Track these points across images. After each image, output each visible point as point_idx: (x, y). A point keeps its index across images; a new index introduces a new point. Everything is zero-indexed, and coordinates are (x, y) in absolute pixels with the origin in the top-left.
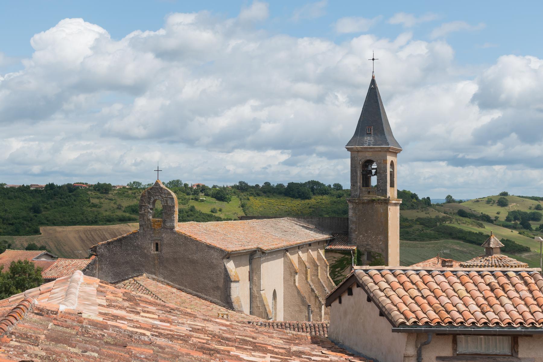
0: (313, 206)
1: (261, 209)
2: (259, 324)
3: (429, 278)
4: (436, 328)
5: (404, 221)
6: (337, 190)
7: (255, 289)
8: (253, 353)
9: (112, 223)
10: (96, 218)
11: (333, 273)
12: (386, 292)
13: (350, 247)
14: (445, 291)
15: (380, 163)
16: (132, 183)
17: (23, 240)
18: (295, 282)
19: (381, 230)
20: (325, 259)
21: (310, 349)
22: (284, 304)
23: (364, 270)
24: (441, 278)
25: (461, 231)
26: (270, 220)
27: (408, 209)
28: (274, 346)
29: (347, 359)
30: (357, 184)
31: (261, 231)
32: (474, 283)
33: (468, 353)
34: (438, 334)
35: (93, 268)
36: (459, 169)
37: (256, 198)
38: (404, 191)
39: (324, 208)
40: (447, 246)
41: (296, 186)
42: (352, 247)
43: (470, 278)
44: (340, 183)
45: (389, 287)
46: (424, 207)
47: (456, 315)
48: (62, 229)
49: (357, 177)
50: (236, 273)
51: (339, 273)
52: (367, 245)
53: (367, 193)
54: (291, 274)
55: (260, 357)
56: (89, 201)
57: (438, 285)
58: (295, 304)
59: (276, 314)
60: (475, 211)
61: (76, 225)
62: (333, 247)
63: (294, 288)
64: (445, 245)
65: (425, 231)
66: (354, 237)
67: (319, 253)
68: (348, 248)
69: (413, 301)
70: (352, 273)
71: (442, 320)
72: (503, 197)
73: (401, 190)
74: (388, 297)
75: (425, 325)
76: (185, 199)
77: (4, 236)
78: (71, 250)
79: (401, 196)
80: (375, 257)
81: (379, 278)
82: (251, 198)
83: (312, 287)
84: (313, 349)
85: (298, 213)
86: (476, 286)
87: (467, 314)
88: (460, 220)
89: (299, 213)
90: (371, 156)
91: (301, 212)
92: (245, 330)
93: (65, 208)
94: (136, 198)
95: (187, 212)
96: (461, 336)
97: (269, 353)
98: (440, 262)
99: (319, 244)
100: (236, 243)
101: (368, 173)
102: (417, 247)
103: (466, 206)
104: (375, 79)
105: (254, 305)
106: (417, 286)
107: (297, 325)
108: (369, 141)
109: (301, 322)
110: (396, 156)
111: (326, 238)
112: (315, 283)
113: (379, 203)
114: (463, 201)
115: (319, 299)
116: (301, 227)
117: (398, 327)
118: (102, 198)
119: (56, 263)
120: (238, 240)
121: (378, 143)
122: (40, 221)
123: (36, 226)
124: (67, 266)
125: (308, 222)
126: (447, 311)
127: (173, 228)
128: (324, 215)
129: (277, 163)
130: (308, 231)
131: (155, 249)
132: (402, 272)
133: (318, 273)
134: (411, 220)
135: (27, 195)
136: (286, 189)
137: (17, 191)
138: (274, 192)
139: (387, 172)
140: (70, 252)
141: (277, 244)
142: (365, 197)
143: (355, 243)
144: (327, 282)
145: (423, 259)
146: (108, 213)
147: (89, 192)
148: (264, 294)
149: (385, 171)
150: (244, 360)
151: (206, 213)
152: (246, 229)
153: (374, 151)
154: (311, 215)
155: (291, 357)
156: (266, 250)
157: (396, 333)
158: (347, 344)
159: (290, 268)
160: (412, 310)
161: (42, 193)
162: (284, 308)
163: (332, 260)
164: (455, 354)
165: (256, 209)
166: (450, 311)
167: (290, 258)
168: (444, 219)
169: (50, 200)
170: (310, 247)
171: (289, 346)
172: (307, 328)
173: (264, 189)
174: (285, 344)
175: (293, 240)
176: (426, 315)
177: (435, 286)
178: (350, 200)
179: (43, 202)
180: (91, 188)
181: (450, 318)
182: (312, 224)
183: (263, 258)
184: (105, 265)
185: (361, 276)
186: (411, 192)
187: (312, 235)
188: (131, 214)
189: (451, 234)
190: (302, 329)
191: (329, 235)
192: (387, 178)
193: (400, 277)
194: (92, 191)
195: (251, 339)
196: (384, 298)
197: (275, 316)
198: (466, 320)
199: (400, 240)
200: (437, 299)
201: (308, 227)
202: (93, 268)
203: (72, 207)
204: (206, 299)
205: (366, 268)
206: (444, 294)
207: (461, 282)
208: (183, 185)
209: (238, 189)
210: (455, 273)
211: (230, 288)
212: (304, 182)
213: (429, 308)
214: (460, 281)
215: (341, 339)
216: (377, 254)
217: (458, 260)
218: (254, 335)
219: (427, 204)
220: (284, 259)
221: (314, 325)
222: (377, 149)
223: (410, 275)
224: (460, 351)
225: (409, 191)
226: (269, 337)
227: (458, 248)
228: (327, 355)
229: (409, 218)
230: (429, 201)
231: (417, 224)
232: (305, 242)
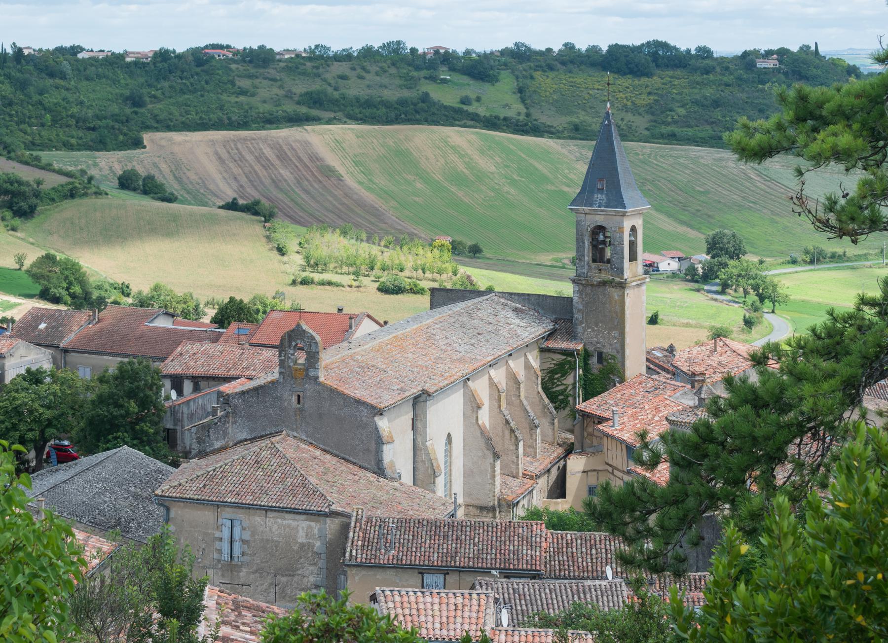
0: (656, 90)
1: (555, 97)
7: (419, 440)
9: (275, 125)
10: (245, 117)
16: (313, 47)
17: (113, 160)
37: (546, 74)
41: (624, 52)
48: (183, 138)
51: (558, 381)
56: (233, 83)
61: (209, 130)
63: (476, 426)
76: (412, 77)
77: (78, 153)
78: (200, 178)
79: (826, 71)
82: (537, 74)
83: (507, 418)
85: (626, 105)
89: (629, 103)
91: (632, 102)
93: (188, 96)
94: (319, 76)
95: (415, 105)
105: (419, 459)
118: (257, 77)
119: (179, 349)
122: (143, 123)
123: (136, 133)
124: (194, 354)
127: (317, 378)
131: (297, 402)
135: (119, 72)
137: (101, 65)
138: (582, 63)
140: (199, 184)
143: (582, 339)
146: (267, 107)
147: (233, 66)
148: (432, 445)
151: (451, 104)
154: (651, 108)
161: (147, 69)
165: (546, 96)
169: (162, 81)
172: (445, 526)
173: (563, 56)
179: (150, 86)
180: (236, 58)
188: (310, 108)
194: (238, 64)
203: (202, 96)
204: (354, 464)
208: (409, 51)
212: (638, 43)
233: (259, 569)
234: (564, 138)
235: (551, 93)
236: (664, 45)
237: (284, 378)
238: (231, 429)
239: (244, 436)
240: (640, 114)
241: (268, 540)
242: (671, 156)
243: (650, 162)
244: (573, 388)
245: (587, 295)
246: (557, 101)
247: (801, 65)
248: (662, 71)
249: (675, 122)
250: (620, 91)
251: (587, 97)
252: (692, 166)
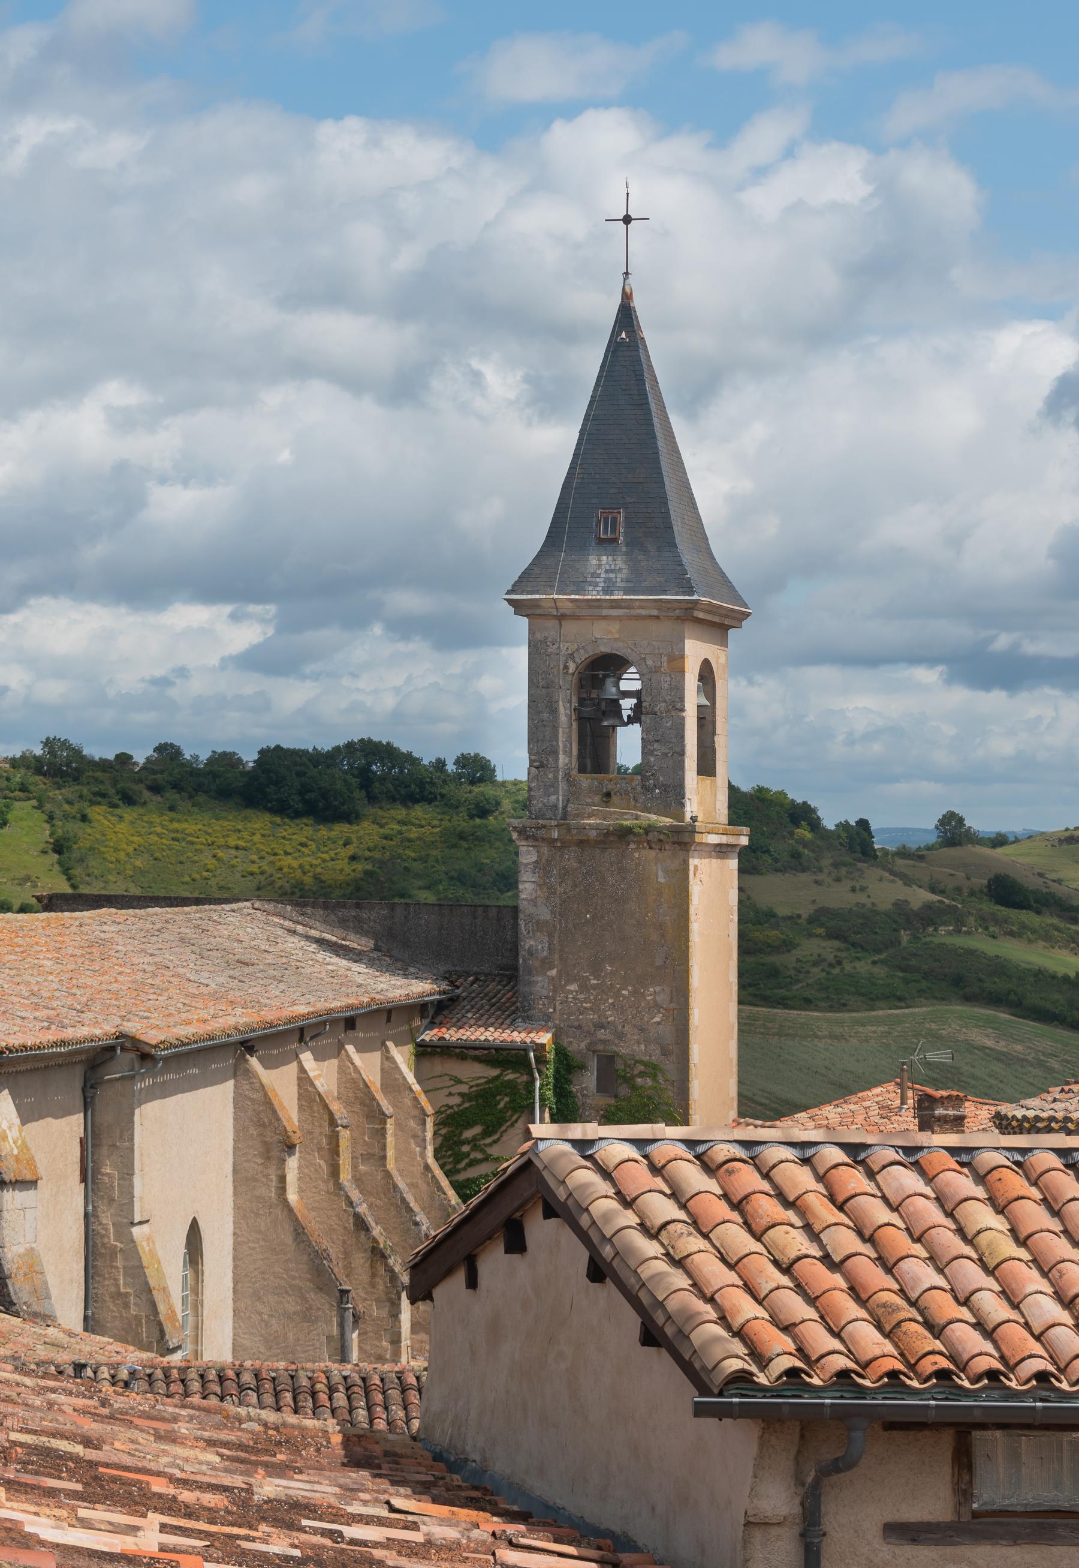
1: (138, 863)
2: (124, 1374)
3: (854, 1180)
4: (885, 1398)
5: (760, 924)
6: (472, 783)
7: (107, 1219)
8: (82, 1513)
11: (450, 1148)
12: (669, 1238)
13: (523, 1035)
14: (922, 1235)
15: (657, 670)
18: (282, 1189)
19: (659, 962)
20: (416, 1087)
21: (337, 1490)
22: (236, 1282)
23: (575, 1143)
24: (908, 1180)
25: (1000, 968)
26: (176, 914)
27: (777, 870)
28: (178, 1480)
29: (498, 1533)
30: (557, 760)
31: (135, 960)
32: (1045, 1200)
33: (1019, 1509)
34: (891, 1426)
36: (995, 699)
37: (118, 811)
38: (760, 790)
39: (415, 860)
40: (944, 1033)
42: (532, 1035)
43: (1028, 1178)
45: (682, 1215)
46: (844, 864)
47: (971, 1341)
49: (555, 728)
50: (24, 1147)
51: (475, 1148)
52: (600, 1026)
53: (597, 799)
54: (268, 1151)
55: (116, 1529)
57: (894, 1209)
58: (282, 1283)
59: (198, 1328)
60: (1059, 881)
62: (452, 1035)
63: (278, 1212)
64: (933, 1026)
65: (848, 967)
66: (544, 992)
67: (388, 1058)
68: (517, 1037)
69: (785, 1280)
70: (523, 1154)
71: (908, 1362)
73: (746, 787)
74: (679, 1263)
75: (834, 1384)
79: (745, 813)
80: (633, 1077)
81: (638, 1177)
82: (98, 813)
84: (350, 1492)
86: (1056, 1213)
87: (1017, 1337)
88: (997, 922)
90: (616, 640)
92: (51, 1405)
96: (989, 1433)
97: (156, 1510)
98: (910, 1102)
99: (389, 1020)
100: (23, 1014)
101: (604, 713)
102: (817, 1037)
103: (1021, 860)
104: (637, 303)
106: (802, 1213)
107: (292, 1377)
108: (607, 571)
109: (309, 1365)
110: (723, 642)
111: (421, 995)
112: (371, 1193)
113: (649, 842)
114: (1012, 839)
115: (386, 1265)
116: (313, 947)
117: (720, 1394)
120: (34, 1000)
121: (646, 584)
125: (343, 923)
126: (929, 1325)
128: (416, 892)
129: (214, 661)
130: (344, 963)
132: (739, 1152)
133: (384, 1148)
134: (790, 918)
138: (199, 788)
139: (683, 710)
141: (205, 1021)
142: (589, 816)
143: (548, 1018)
144: (424, 1187)
145: (841, 1086)
148: (149, 1239)
149: (678, 706)
150: (43, 1543)
152: (70, 951)
153: (630, 618)
154: (358, 889)
155: (250, 1528)
156: (155, 1047)
157: (712, 1422)
158: (500, 1466)
159: (263, 1125)
160: (782, 1317)
162: (235, 1301)
163: (446, 1091)
164: (963, 1510)
165: (118, 861)
166: (942, 1322)
167: (264, 1081)
168: (929, 916)
170: (350, 1033)
171: (246, 1479)
172: (332, 1390)
173: (154, 772)
174: (226, 1470)
175: (276, 1002)
176: (842, 1341)
177: (881, 1214)
178: (524, 827)
181: (941, 1353)
182: (360, 931)
183: (143, 1080)
185: (562, 1167)
186: (790, 796)
187: (360, 980)
189: (958, 981)
190: (314, 1394)
191: (434, 981)
192: (683, 737)
193: (730, 1172)
195: (79, 1449)
196: (662, 1266)
197: (197, 1339)
198: (1012, 1362)
199: (740, 1002)
200: (889, 1270)
201: (342, 946)
205: (584, 1132)
206: (918, 1249)
207: (990, 1199)
209: (39, 771)
210: (965, 1158)
212: (325, 745)
213: (853, 1310)
214: (988, 1190)
215: (473, 1446)
216: (642, 1068)
217: (988, 1093)
218: (91, 1427)
219: (858, 848)
220: (235, 1086)
221: (364, 1379)
222: (641, 607)
223: (774, 1166)
224: (986, 1497)
225: (782, 793)
226: (159, 1437)
227: (989, 1043)
228: (410, 1518)
229: (782, 911)
230: (865, 834)
231: (817, 936)
232: (330, 1011)
235: (128, 854)
245: (564, 874)
246: (142, 872)
248: (381, 808)
250: (286, 853)
251: (211, 863)
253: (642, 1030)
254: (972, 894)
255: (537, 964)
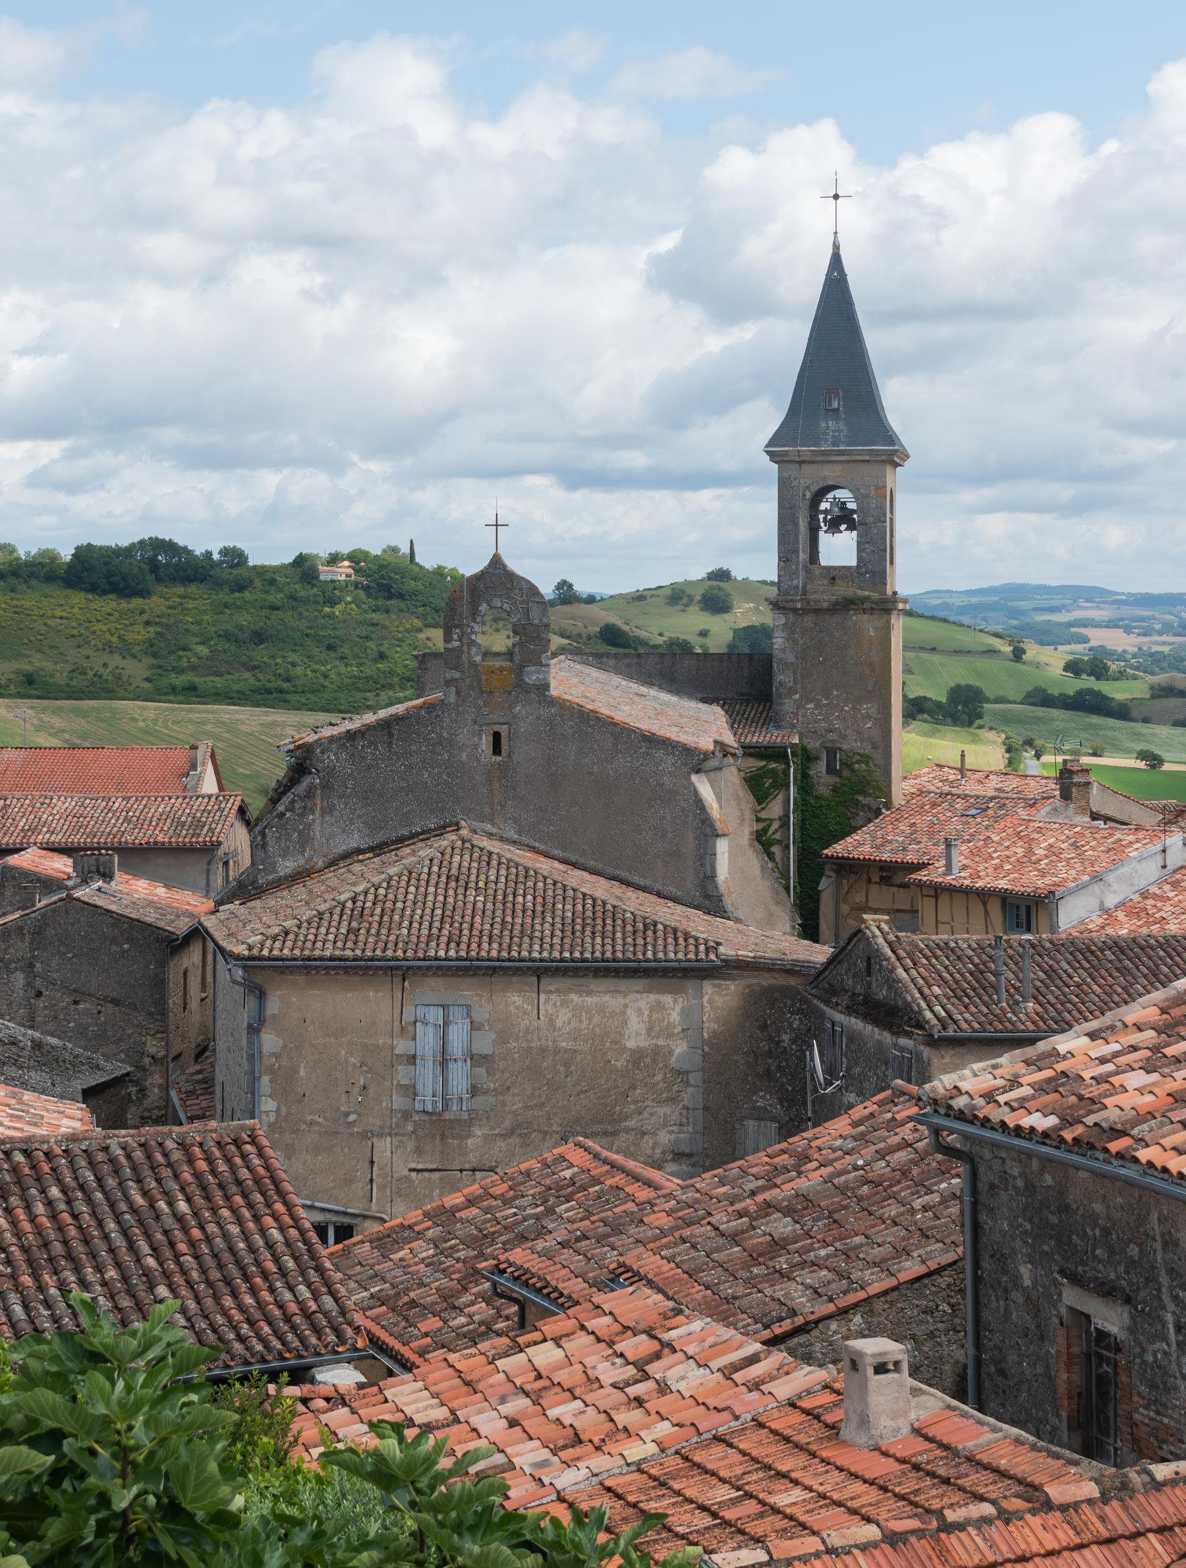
15: (867, 496)
19: (870, 688)
30: (798, 556)
35: (305, 808)
38: (720, 569)
44: (239, 545)
49: (797, 536)
53: (826, 581)
72: (715, 583)
80: (853, 764)
89: (114, 639)
91: (119, 637)
104: (842, 252)
114: (598, 598)
128: (193, 647)
136: (71, 565)
138: (32, 575)
143: (793, 726)
154: (152, 645)
184: (340, 797)
186: (461, 571)
202: (305, 808)
204: (644, 889)
211: (715, 855)
212: (125, 542)
233: (520, 1125)
234: (10, 696)
236: (169, 547)
237: (458, 693)
238: (318, 825)
239: (354, 842)
240: (134, 656)
241: (543, 1050)
242: (190, 721)
243: (157, 731)
244: (781, 827)
247: (392, 575)
249: (193, 668)
250: (98, 621)
251: (43, 629)
252: (225, 735)
253: (859, 733)
254: (589, 638)
255: (785, 691)
